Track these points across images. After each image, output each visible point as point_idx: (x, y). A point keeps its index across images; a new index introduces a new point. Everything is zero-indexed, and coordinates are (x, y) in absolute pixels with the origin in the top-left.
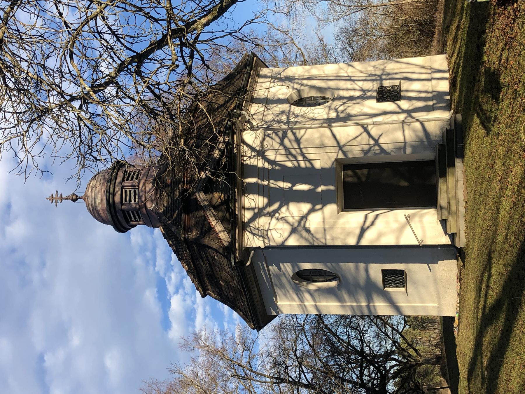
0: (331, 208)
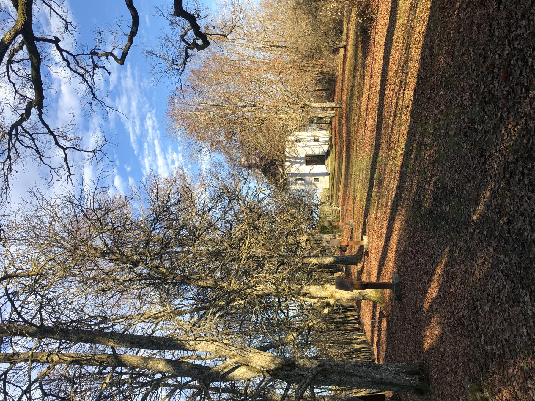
0: (304, 165)
